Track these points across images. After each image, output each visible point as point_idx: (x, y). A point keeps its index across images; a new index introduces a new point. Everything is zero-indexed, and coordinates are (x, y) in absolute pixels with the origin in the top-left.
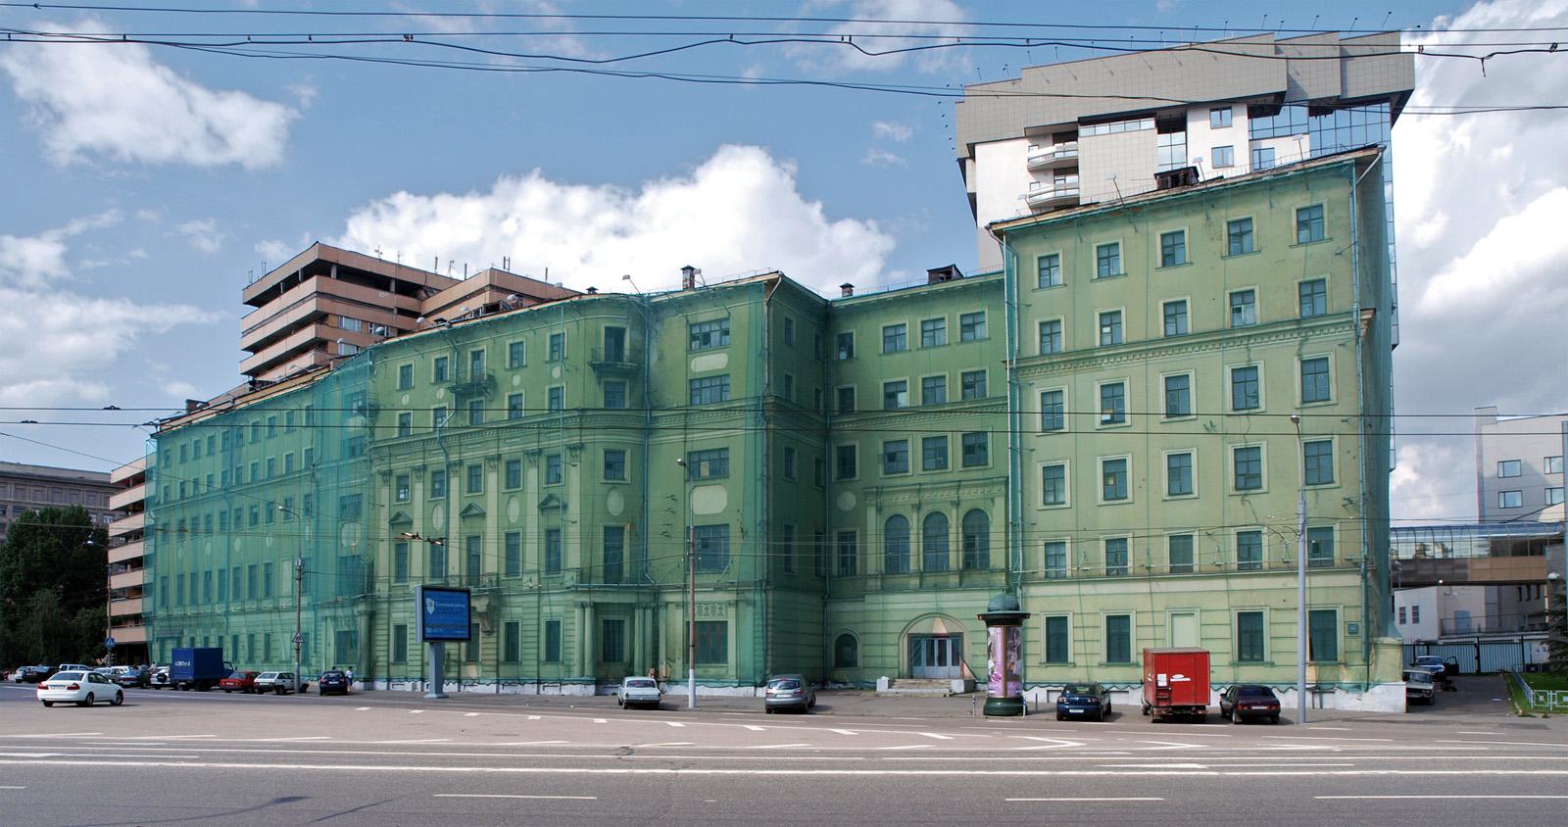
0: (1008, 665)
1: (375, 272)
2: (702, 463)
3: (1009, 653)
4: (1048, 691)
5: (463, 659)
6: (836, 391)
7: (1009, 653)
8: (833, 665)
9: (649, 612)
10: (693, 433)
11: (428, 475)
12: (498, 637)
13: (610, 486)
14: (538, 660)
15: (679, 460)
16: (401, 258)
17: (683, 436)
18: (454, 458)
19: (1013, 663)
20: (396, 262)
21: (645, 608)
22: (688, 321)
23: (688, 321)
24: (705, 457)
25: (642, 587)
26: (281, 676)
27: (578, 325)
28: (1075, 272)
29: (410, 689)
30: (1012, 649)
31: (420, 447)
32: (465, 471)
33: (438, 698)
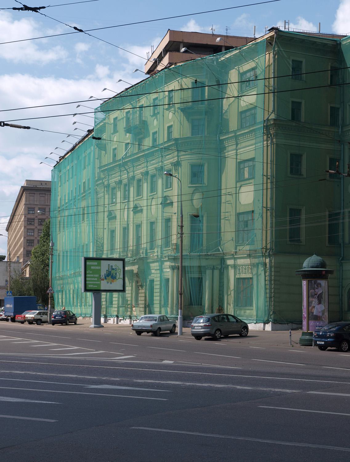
0: (310, 308)
1: (209, 43)
2: (245, 169)
3: (311, 299)
4: (188, 322)
5: (134, 304)
6: (348, 106)
7: (311, 299)
8: (346, 309)
9: (217, 273)
10: (197, 152)
11: (122, 186)
12: (146, 289)
13: (195, 188)
14: (160, 304)
15: (165, 172)
16: (228, 31)
17: (235, 151)
18: (131, 174)
19: (314, 307)
20: (225, 34)
21: (213, 269)
22: (239, 72)
23: (239, 72)
24: (246, 164)
25: (67, 258)
26: (39, 314)
27: (178, 81)
28: (171, 46)
29: (112, 323)
30: (313, 296)
31: (117, 169)
32: (135, 183)
33: (94, 327)
